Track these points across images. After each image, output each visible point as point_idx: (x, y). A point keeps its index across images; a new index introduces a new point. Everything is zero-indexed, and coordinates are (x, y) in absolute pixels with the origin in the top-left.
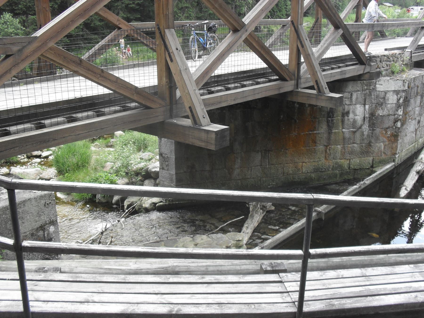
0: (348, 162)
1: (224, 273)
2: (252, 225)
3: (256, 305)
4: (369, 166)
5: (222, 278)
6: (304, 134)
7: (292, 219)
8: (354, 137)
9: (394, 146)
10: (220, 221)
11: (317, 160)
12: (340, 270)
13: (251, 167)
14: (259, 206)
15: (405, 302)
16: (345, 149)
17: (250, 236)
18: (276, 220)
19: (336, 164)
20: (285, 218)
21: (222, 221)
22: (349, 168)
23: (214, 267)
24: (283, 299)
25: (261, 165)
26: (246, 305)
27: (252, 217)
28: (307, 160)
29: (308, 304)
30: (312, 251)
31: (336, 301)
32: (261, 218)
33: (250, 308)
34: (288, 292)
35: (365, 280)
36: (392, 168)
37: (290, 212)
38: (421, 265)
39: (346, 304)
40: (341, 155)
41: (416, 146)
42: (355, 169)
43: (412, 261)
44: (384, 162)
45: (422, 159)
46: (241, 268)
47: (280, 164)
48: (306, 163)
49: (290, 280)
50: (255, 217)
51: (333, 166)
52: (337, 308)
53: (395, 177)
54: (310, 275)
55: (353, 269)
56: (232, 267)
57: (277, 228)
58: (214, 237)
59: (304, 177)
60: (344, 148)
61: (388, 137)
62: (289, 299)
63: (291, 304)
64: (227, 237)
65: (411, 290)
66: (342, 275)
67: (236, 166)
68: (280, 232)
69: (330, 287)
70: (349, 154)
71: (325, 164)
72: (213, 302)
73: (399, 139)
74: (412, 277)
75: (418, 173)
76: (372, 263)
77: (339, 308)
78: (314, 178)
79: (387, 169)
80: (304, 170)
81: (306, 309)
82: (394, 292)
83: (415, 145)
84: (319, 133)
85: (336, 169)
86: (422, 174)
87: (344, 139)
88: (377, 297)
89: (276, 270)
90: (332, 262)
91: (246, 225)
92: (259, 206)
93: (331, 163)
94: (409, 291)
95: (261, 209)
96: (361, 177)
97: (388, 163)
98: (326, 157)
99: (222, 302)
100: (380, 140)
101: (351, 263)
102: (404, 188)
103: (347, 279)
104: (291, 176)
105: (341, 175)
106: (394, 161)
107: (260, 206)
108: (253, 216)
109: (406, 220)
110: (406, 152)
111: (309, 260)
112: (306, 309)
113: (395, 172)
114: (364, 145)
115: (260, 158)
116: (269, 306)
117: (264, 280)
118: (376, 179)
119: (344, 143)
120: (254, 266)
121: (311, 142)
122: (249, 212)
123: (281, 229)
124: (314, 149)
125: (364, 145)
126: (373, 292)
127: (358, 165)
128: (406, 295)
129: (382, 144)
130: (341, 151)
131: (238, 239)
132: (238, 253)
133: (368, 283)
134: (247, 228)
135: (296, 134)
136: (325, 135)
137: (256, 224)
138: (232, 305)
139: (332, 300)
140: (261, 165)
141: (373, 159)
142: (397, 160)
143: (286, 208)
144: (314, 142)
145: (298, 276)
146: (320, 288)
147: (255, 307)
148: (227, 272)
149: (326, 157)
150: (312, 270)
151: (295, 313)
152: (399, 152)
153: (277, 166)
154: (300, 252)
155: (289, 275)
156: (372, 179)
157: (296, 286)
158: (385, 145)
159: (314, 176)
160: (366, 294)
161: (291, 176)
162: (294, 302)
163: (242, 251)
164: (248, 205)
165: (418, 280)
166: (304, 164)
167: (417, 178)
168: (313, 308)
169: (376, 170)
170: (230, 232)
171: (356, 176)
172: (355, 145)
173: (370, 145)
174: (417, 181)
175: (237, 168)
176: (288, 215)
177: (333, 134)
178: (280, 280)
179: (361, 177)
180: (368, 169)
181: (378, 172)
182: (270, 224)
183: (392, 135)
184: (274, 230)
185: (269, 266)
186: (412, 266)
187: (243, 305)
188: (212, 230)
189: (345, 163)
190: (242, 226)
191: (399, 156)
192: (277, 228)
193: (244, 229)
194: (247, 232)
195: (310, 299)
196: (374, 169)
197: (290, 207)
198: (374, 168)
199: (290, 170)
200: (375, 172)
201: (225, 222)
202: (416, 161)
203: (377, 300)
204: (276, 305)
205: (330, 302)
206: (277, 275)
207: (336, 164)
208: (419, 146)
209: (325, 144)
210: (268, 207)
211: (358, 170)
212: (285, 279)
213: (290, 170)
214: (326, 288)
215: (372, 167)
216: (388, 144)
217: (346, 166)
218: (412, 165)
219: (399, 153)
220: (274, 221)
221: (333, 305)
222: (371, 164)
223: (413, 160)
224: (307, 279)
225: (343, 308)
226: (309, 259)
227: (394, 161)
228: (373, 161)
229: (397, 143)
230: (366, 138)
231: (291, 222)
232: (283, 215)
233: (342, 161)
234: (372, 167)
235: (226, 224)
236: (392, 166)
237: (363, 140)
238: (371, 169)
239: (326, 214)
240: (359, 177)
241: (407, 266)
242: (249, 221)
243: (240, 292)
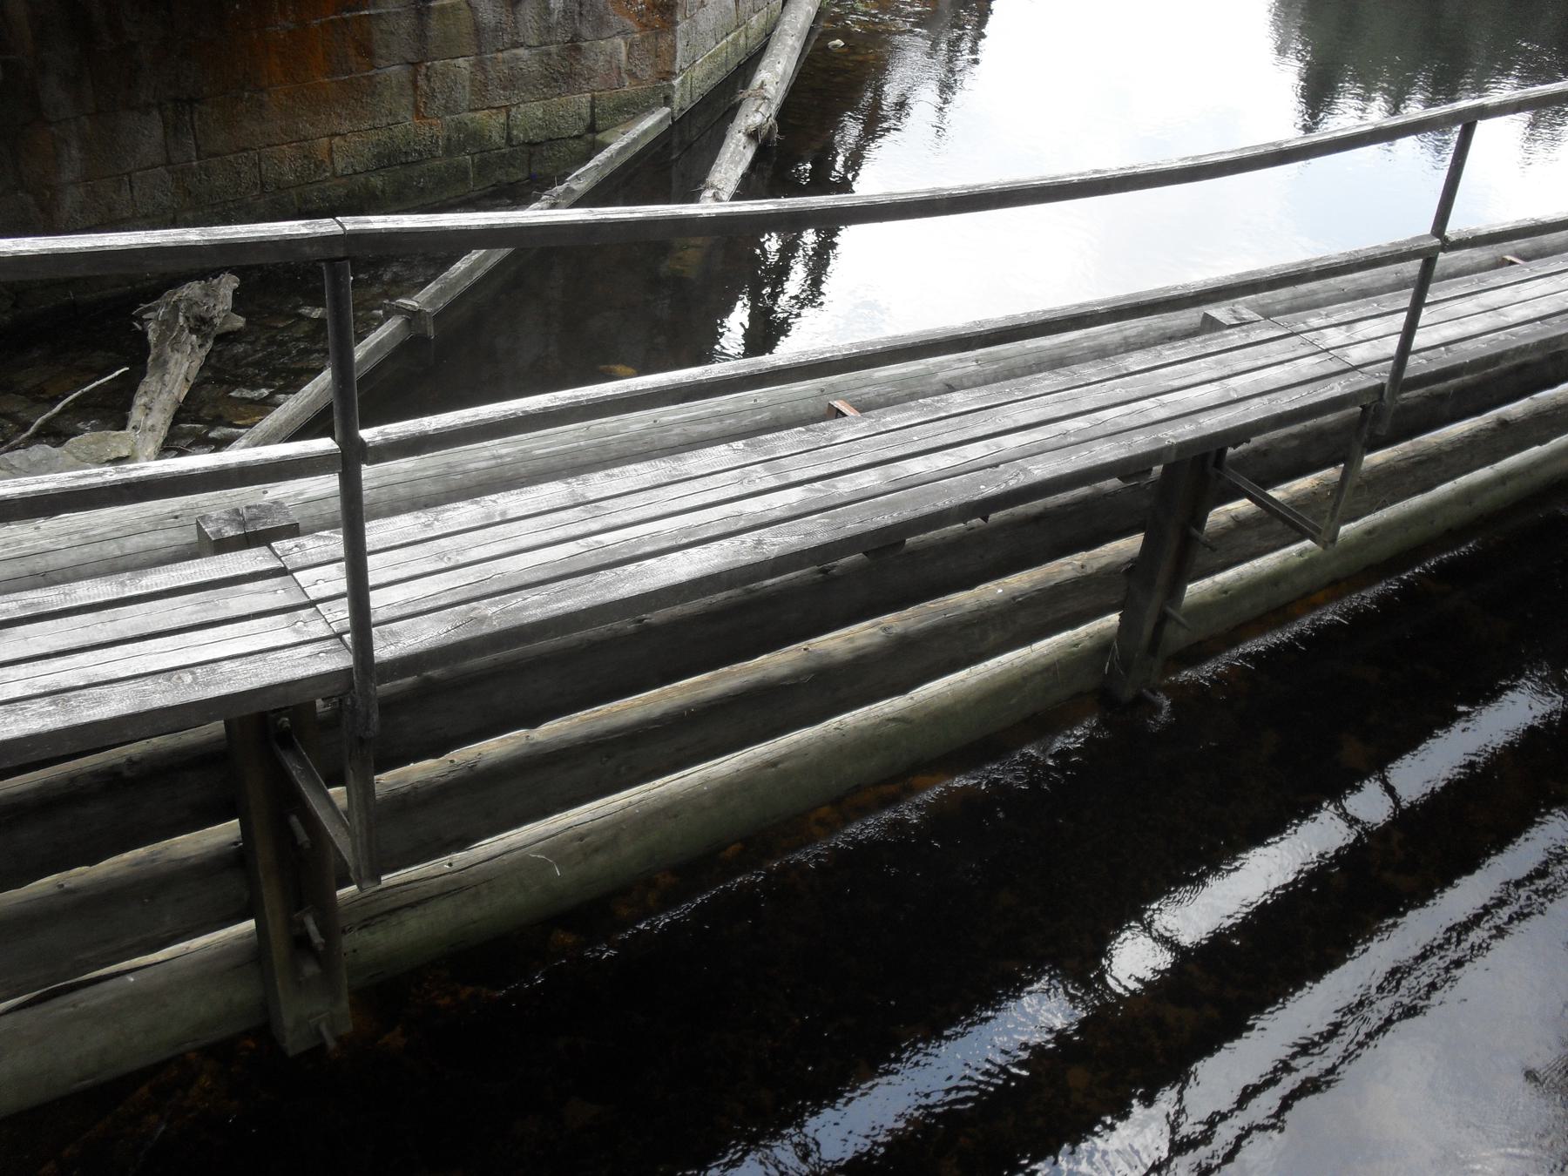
0: (502, 119)
1: (59, 577)
2: (164, 396)
3: (198, 670)
4: (582, 125)
5: (52, 598)
6: (321, 25)
7: (318, 351)
8: (516, 22)
9: (663, 44)
10: (37, 401)
11: (384, 123)
12: (494, 497)
13: (129, 174)
14: (181, 320)
15: (724, 568)
16: (484, 71)
17: (166, 440)
18: (256, 364)
19: (458, 130)
20: (289, 353)
21: (45, 401)
22: (509, 139)
23: (16, 562)
24: (297, 631)
25: (169, 162)
26: (161, 679)
27: (162, 364)
28: (346, 126)
29: (392, 633)
30: (368, 435)
31: (491, 604)
32: (197, 364)
33: (177, 686)
34: (312, 604)
35: (584, 516)
36: (664, 127)
37: (305, 327)
38: (769, 436)
39: (525, 608)
40: (473, 93)
41: (742, 41)
42: (531, 144)
43: (741, 430)
44: (633, 109)
45: (762, 85)
46: (121, 547)
47: (244, 150)
48: (343, 135)
49: (316, 560)
50: (171, 364)
51: (449, 139)
52: (497, 628)
53: (677, 160)
54: (377, 532)
55: (544, 486)
56: (86, 549)
57: (265, 392)
58: (15, 463)
59: (342, 191)
60: (480, 65)
61: (640, 14)
62: (318, 629)
63: (328, 643)
64: (70, 452)
65: (741, 524)
66: (504, 513)
67: (67, 176)
68: (278, 405)
69: (462, 560)
70: (504, 89)
71: (417, 135)
72: (29, 692)
73: (679, 18)
74: (741, 482)
75: (752, 135)
76: (606, 457)
77: (504, 626)
78: (383, 192)
79: (645, 133)
80: (340, 165)
81: (384, 651)
82: (685, 541)
83: (735, 40)
84: (379, 15)
85: (462, 147)
86: (767, 140)
87: (478, 30)
88: (631, 567)
89: (256, 533)
90: (464, 472)
91: (140, 401)
92: (181, 320)
93: (437, 128)
94: (734, 528)
95: (192, 331)
96: (557, 169)
97: (648, 110)
98: (417, 109)
99: (64, 685)
100: (611, 27)
101: (531, 466)
102: (709, 193)
103: (522, 522)
104: (293, 192)
105: (483, 167)
106: (667, 101)
107: (187, 318)
108: (166, 362)
109: (728, 310)
110: (707, 67)
111: (367, 471)
112: (384, 651)
113: (676, 140)
114: (553, 49)
115: (158, 132)
116: (250, 667)
117: (217, 576)
118: (607, 172)
119: (479, 47)
120: (172, 533)
121: (352, 52)
122: (145, 349)
123: (281, 397)
124: (370, 78)
125: (553, 49)
126: (614, 552)
127: (540, 127)
128: (726, 543)
129: (619, 41)
130: (472, 81)
131: (113, 456)
132: (83, 482)
133: (595, 526)
134: (148, 408)
135: (292, 26)
136: (406, 23)
137: (180, 391)
138: (105, 690)
139: (474, 604)
140: (169, 162)
141: (593, 98)
142: (677, 97)
143: (289, 317)
144: (366, 51)
145: (334, 542)
146: (429, 569)
147: (195, 679)
148: (69, 574)
149: (417, 109)
150: (395, 509)
151: (347, 672)
152: (685, 66)
153: (231, 157)
154: (324, 444)
155: (308, 542)
156: (594, 174)
157: (334, 579)
158: (631, 46)
159: (379, 184)
160: (593, 562)
161: (293, 192)
162: (339, 636)
163: (98, 475)
164: (142, 322)
165: (761, 487)
166: (337, 139)
167: (749, 154)
168: (412, 641)
169: (608, 140)
170: (82, 432)
171: (536, 169)
172: (522, 52)
173: (578, 49)
174: (753, 165)
175: (72, 183)
176: (298, 340)
177: (435, 16)
178: (276, 564)
179: (557, 169)
180: (578, 137)
181: (615, 147)
182: (235, 385)
183: (655, 6)
184: (252, 401)
185: (229, 522)
186: (740, 444)
187: (149, 681)
188: (7, 441)
189: (491, 123)
190: (129, 405)
191: (683, 83)
192: (265, 392)
193: (136, 415)
194: (149, 423)
195: (398, 613)
196: (599, 137)
197: (305, 311)
198: (598, 132)
199: (286, 169)
200: (605, 146)
201: (55, 401)
202: (746, 93)
203: (632, 575)
204: (272, 656)
205: (467, 612)
206: (264, 550)
207: (458, 130)
208: (751, 43)
209: (411, 57)
210: (217, 321)
211: (540, 144)
212: (297, 558)
213: (286, 169)
214: (451, 564)
215: (592, 128)
216: (643, 41)
217: (496, 137)
218: (732, 112)
219: (682, 70)
220: (250, 371)
221: (482, 620)
222: (588, 120)
223: (734, 92)
224: (369, 548)
225: (517, 623)
226: (364, 466)
227: (667, 101)
228: (593, 107)
229: (674, 32)
230: (558, 23)
231: (316, 364)
232: (282, 344)
233: (478, 115)
234: (592, 128)
235: (59, 407)
236: (661, 121)
237: (549, 29)
238: (589, 137)
239: (439, 317)
240: (549, 171)
241: (723, 447)
242: (150, 382)
243: (130, 634)
